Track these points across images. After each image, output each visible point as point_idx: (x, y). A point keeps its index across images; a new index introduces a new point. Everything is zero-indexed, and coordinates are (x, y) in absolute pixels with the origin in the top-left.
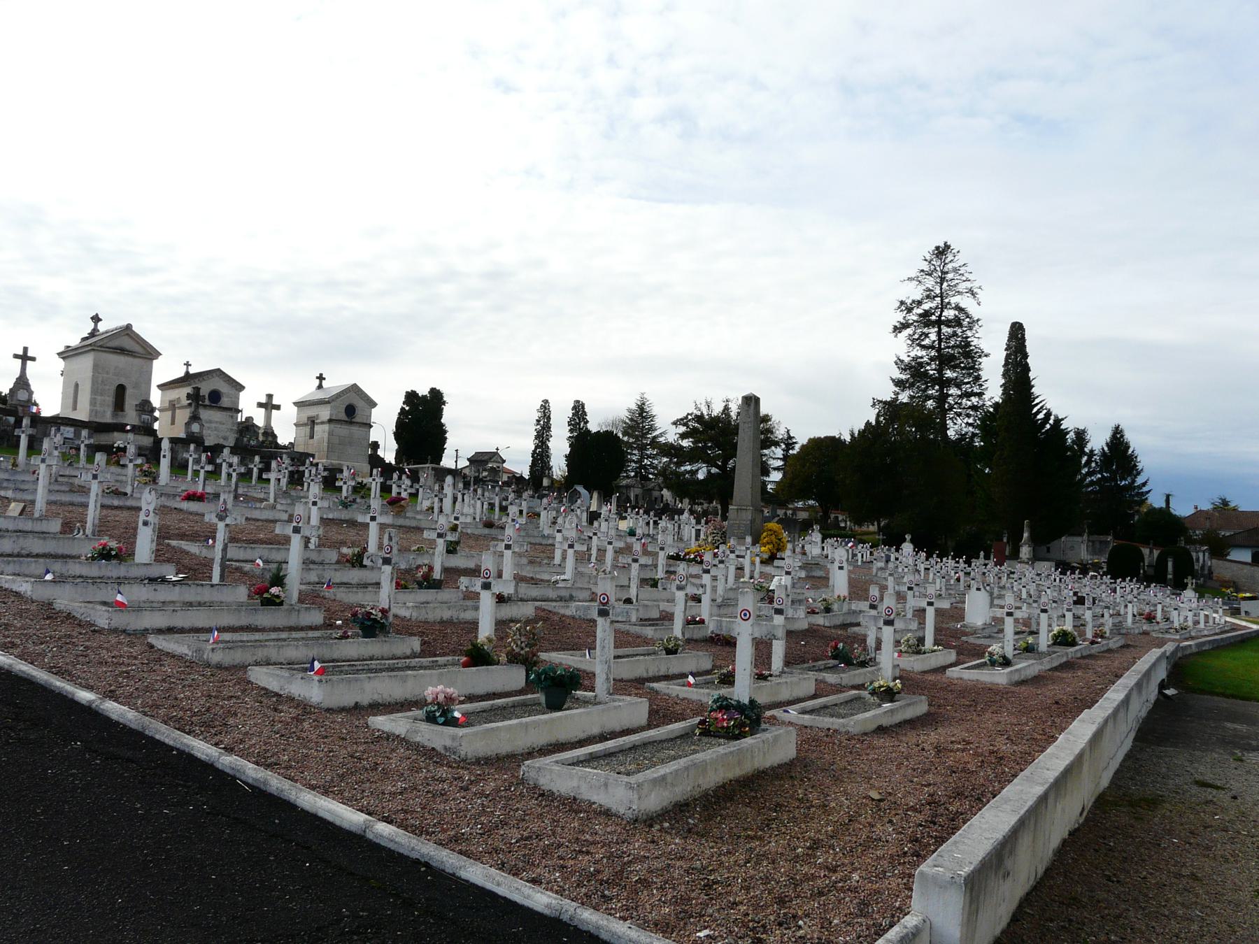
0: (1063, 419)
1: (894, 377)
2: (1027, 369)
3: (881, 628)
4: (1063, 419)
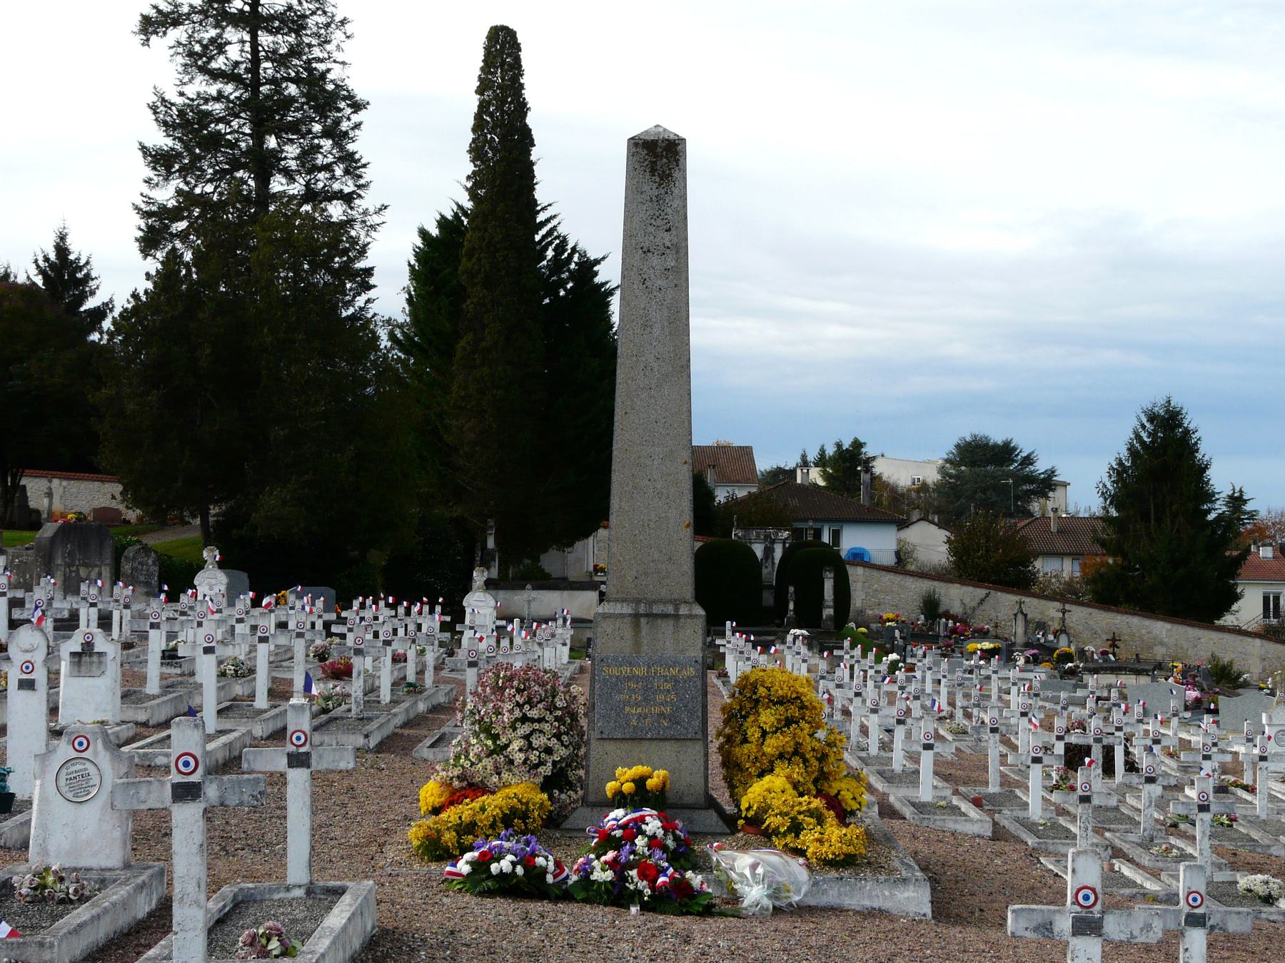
0: (597, 262)
1: (149, 144)
2: (526, 139)
3: (255, 646)
4: (597, 262)
